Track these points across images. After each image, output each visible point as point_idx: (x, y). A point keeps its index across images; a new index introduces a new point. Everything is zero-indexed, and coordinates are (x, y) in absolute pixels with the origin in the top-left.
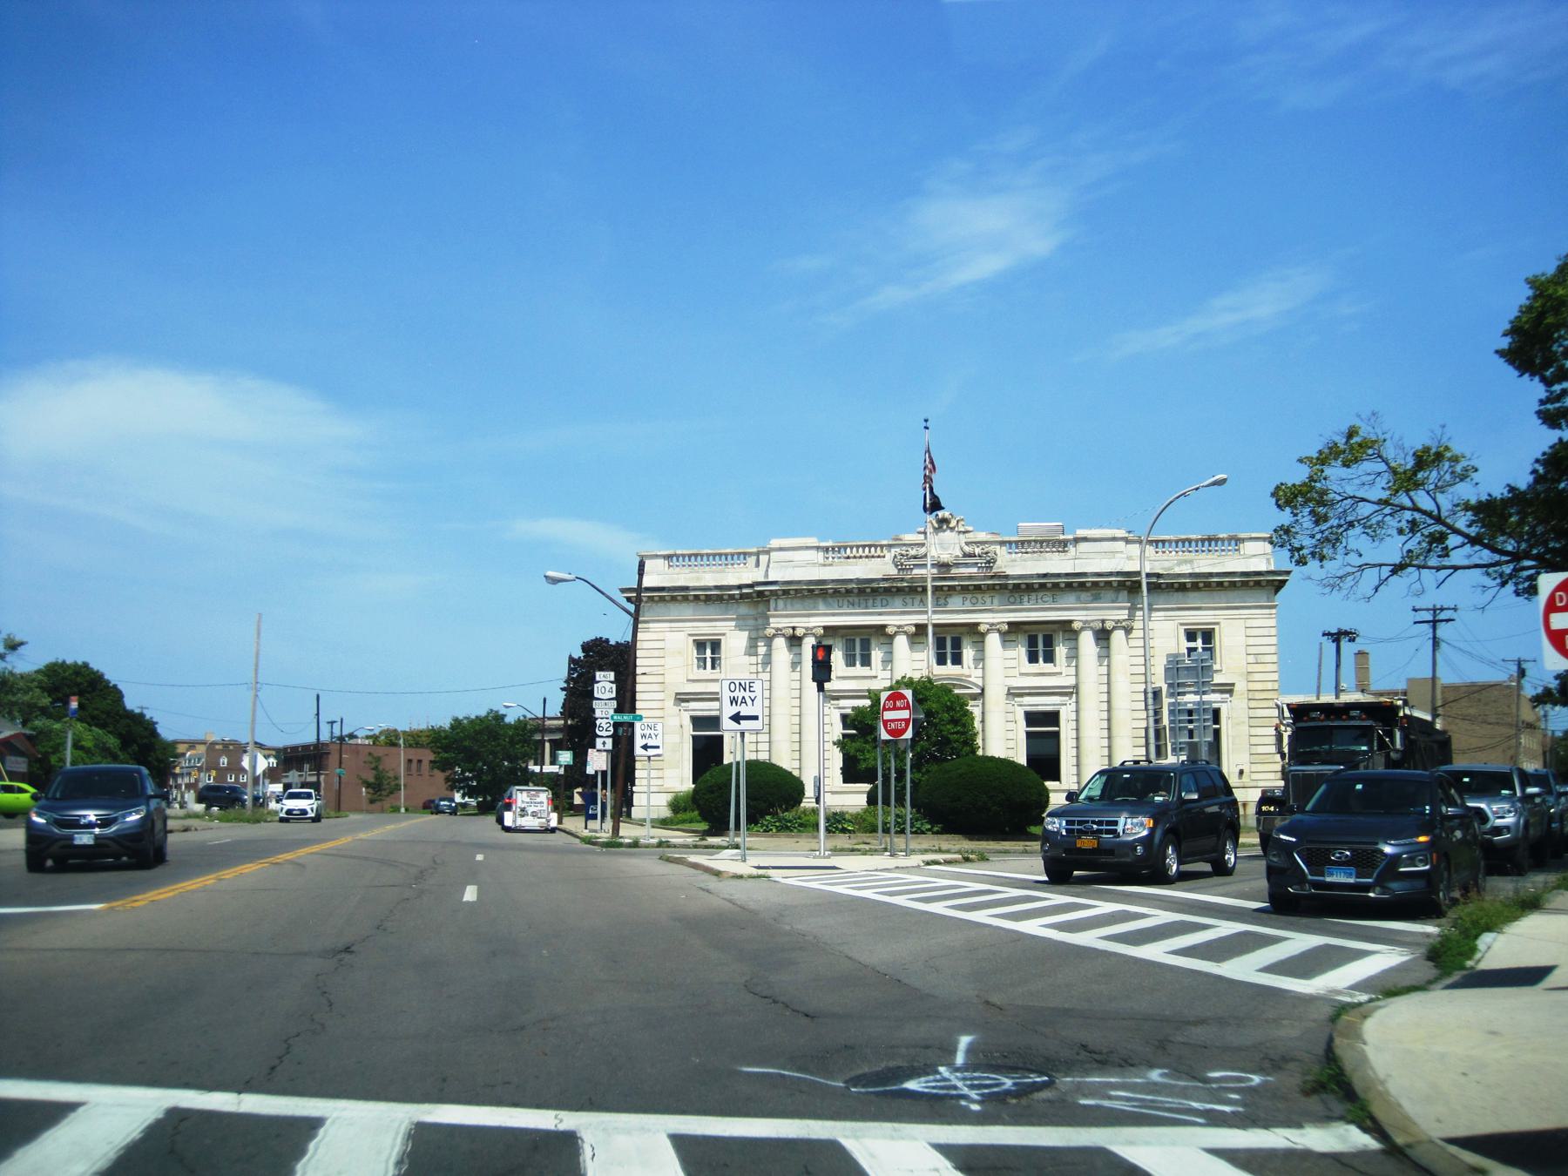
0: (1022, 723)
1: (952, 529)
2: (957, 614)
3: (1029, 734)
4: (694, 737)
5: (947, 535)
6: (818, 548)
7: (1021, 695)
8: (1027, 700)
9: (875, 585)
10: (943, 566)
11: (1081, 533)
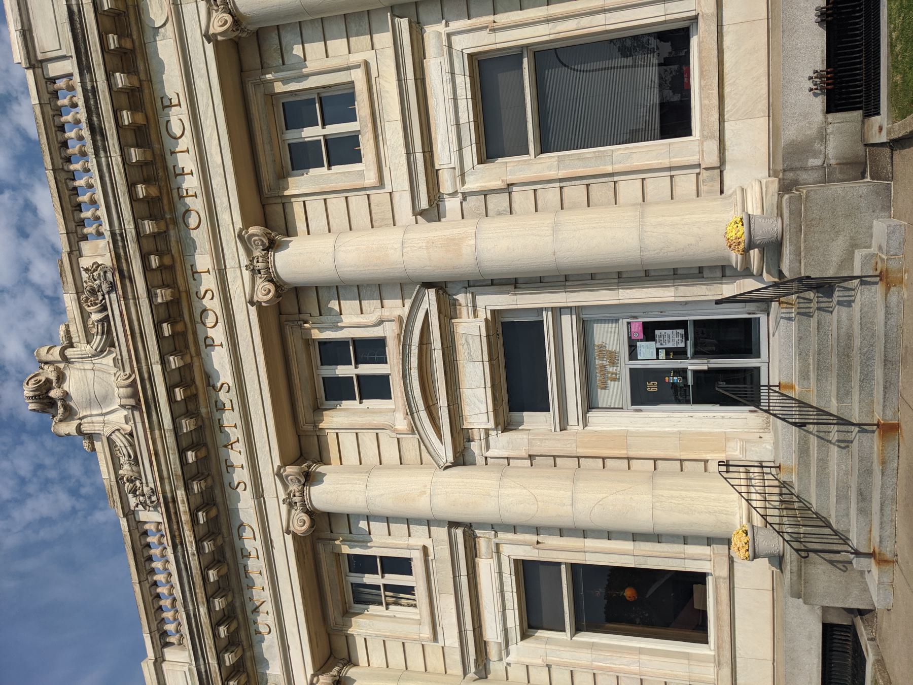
0: (508, 168)
1: (61, 378)
2: (237, 358)
3: (544, 148)
4: (578, 628)
5: (76, 384)
6: (159, 661)
7: (481, 646)
8: (444, 156)
9: (194, 563)
10: (140, 400)
11: (18, 54)
